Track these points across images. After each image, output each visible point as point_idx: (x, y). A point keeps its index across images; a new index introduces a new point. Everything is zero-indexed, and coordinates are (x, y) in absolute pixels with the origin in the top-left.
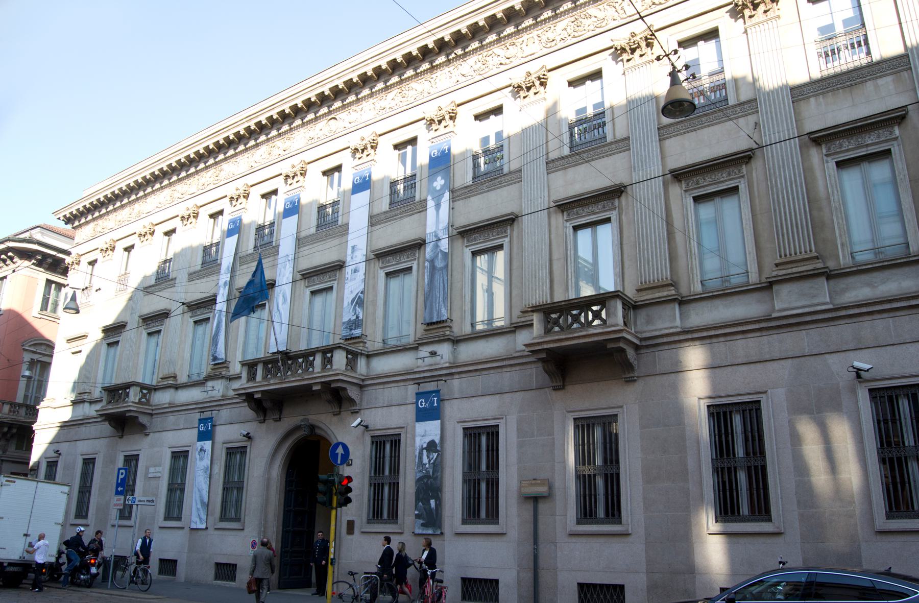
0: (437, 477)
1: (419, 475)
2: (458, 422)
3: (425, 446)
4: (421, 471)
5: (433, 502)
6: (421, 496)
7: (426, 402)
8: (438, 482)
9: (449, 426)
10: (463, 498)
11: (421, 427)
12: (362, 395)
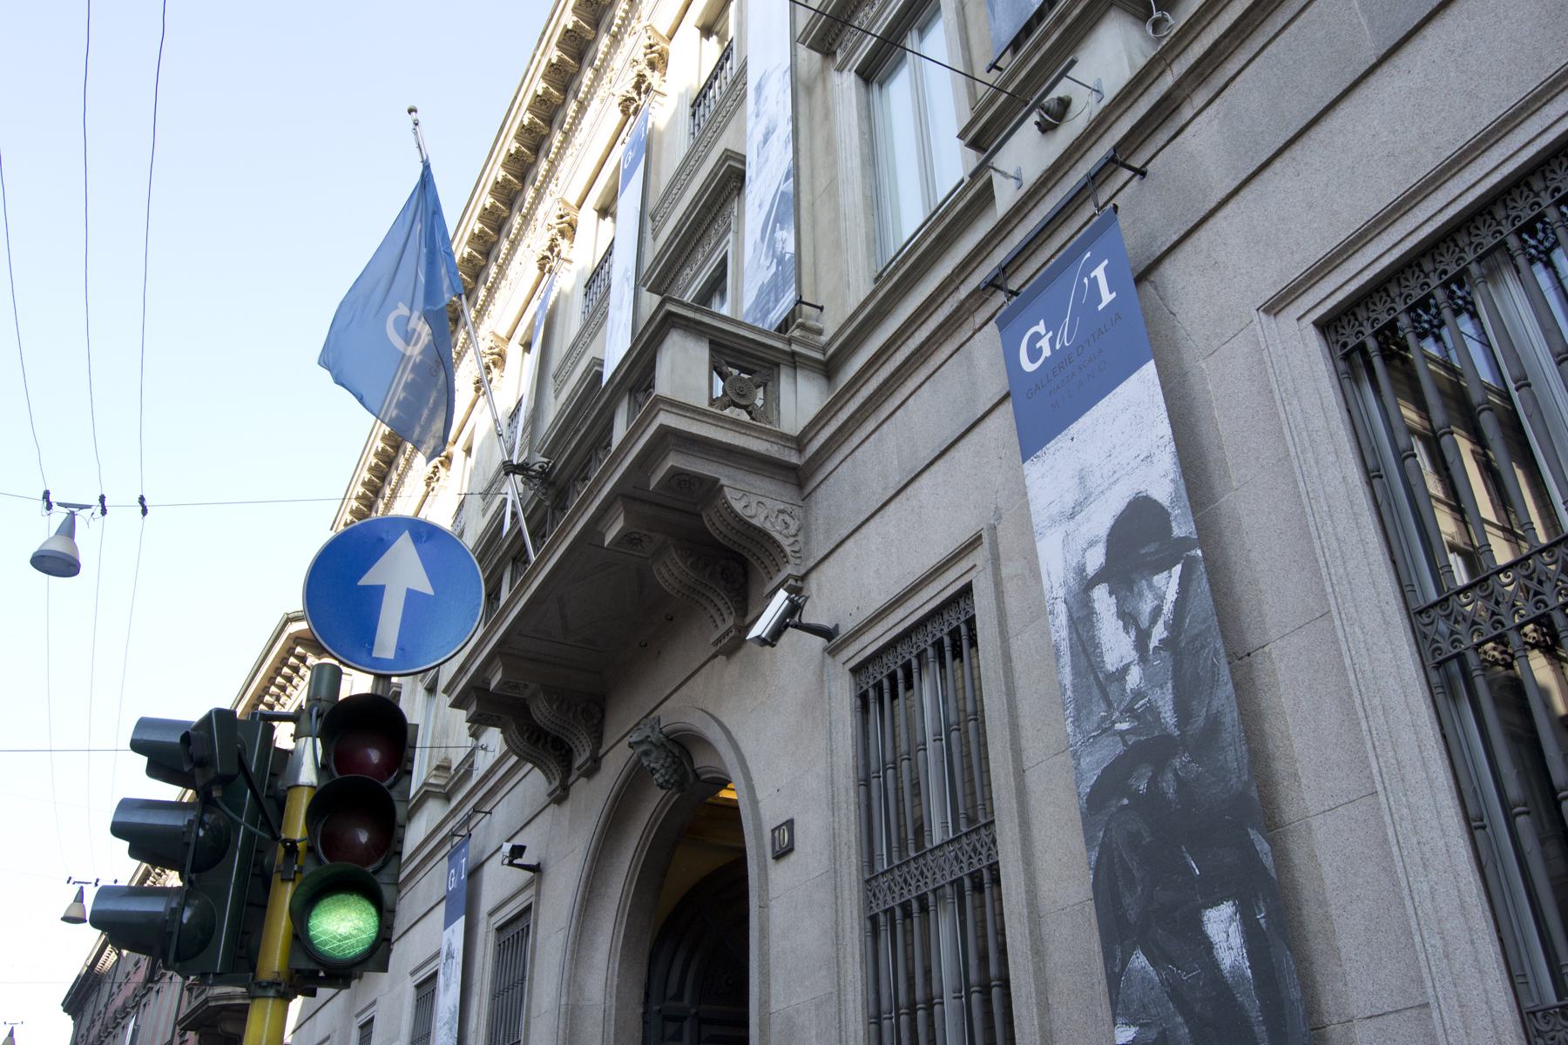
0: (1214, 724)
1: (1094, 763)
2: (1274, 307)
3: (1095, 560)
4: (1106, 729)
5: (1222, 926)
6: (1132, 906)
7: (1052, 326)
8: (1233, 756)
9: (1222, 382)
10: (1474, 824)
11: (1050, 478)
12: (807, 511)
